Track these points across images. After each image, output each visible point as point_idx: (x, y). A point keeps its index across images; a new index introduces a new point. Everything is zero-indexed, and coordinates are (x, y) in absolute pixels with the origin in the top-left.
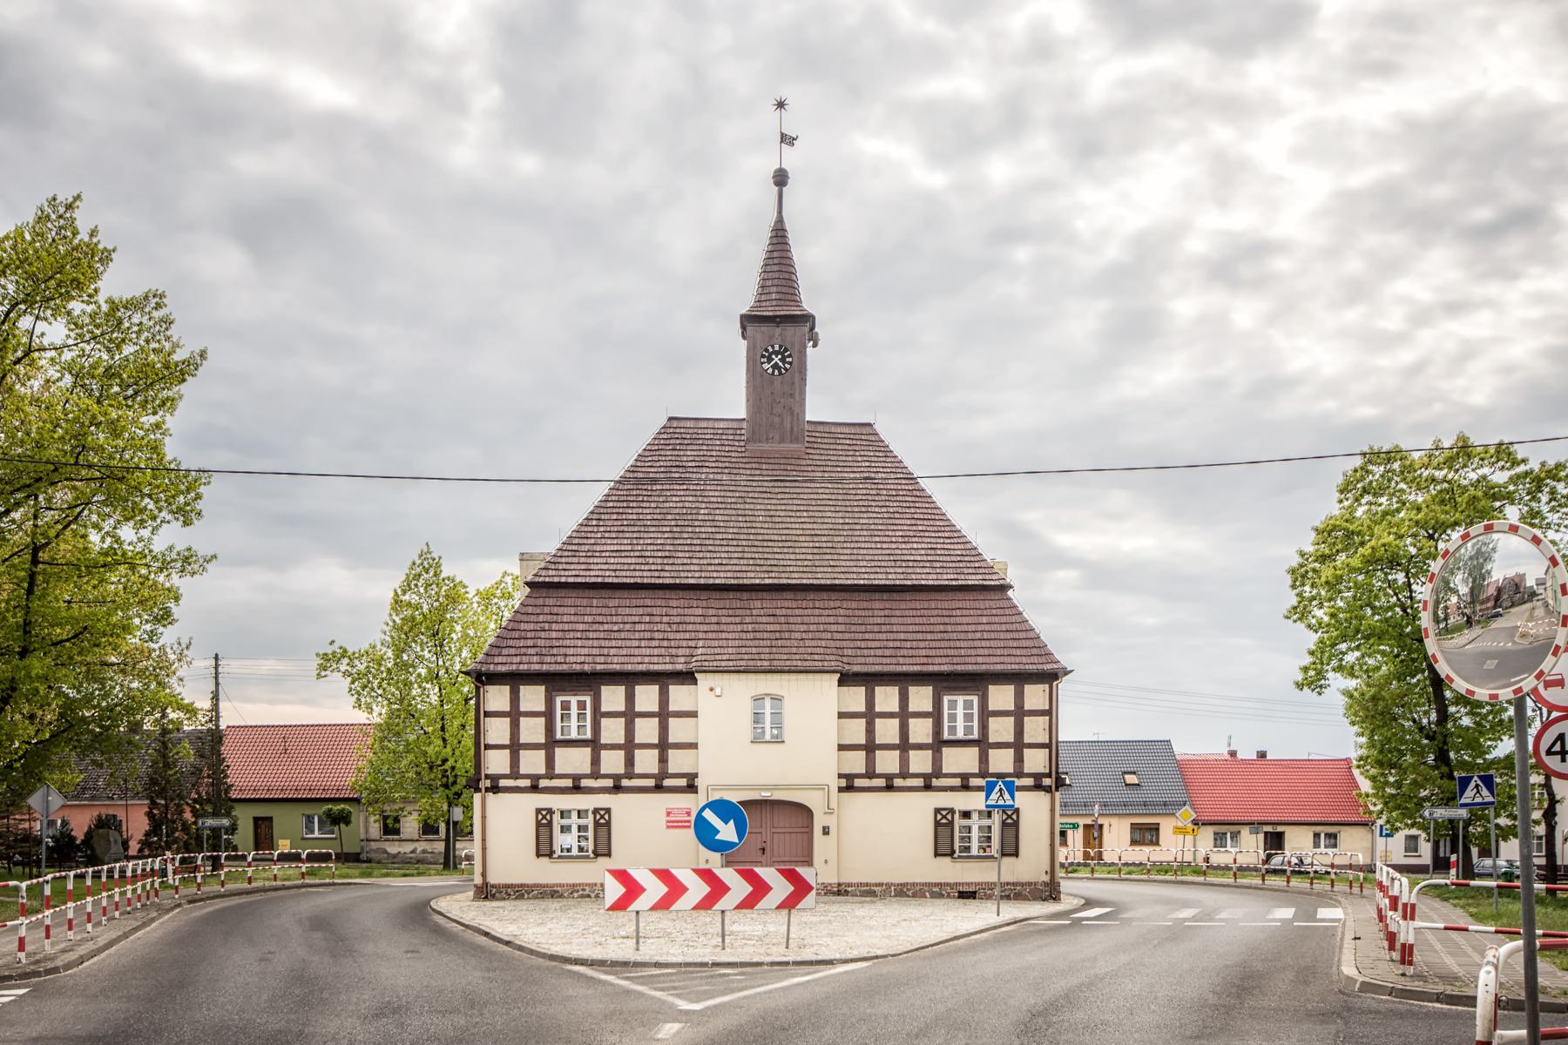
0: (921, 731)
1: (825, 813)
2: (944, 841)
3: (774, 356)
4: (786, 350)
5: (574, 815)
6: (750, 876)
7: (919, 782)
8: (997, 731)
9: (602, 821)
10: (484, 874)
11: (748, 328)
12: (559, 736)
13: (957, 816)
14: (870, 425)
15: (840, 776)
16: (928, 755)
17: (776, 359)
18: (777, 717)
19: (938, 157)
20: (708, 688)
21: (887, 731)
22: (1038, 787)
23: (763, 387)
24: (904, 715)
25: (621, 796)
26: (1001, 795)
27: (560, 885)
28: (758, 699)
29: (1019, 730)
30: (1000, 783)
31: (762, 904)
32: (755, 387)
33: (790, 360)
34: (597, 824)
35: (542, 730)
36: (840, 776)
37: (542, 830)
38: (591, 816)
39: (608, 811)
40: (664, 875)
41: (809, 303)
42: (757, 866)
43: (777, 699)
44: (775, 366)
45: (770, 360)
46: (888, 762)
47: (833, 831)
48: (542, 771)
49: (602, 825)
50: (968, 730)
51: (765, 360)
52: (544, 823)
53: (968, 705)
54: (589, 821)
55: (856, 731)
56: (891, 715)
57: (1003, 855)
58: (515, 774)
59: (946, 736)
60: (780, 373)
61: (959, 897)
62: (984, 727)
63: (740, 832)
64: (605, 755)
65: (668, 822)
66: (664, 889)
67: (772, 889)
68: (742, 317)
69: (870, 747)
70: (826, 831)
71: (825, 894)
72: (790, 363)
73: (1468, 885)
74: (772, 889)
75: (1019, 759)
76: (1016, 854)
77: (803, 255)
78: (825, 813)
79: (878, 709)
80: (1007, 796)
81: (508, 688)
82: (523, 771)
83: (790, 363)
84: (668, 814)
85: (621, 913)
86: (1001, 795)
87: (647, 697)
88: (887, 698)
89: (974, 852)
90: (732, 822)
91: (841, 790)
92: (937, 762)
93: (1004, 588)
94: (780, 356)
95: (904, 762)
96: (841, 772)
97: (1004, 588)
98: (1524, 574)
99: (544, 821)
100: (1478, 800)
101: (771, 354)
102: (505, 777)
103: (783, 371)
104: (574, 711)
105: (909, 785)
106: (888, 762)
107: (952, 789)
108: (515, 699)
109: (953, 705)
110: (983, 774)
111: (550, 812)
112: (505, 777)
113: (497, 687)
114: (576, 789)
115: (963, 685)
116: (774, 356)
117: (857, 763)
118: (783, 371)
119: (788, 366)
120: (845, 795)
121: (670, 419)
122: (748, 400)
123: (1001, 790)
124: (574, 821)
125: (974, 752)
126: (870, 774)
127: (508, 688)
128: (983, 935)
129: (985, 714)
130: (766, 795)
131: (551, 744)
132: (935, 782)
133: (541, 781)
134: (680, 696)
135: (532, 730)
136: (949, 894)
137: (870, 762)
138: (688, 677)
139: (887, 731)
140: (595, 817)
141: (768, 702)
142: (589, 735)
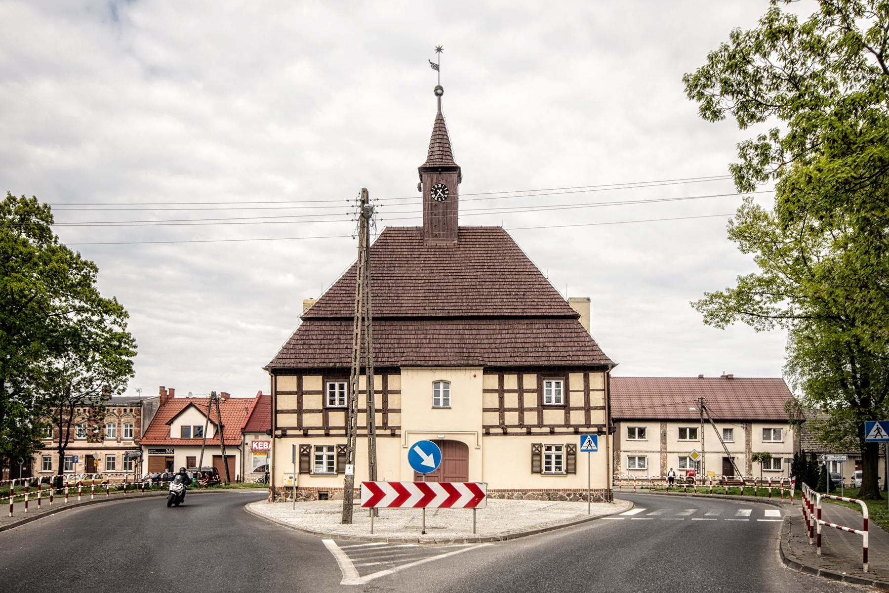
1: (476, 448)
3: (438, 190)
4: (445, 187)
6: (448, 487)
11: (423, 176)
12: (545, 403)
17: (440, 192)
18: (446, 393)
24: (587, 391)
28: (437, 383)
29: (521, 400)
30: (589, 437)
31: (405, 505)
33: (447, 192)
34: (568, 454)
36: (484, 427)
37: (303, 458)
38: (335, 449)
40: (397, 486)
41: (458, 160)
42: (455, 481)
43: (447, 383)
45: (436, 193)
50: (558, 400)
51: (433, 193)
52: (304, 454)
53: (342, 387)
54: (563, 452)
55: (493, 400)
57: (301, 473)
58: (541, 425)
60: (442, 200)
61: (320, 498)
63: (436, 461)
66: (422, 495)
67: (461, 495)
68: (419, 169)
69: (502, 410)
72: (447, 194)
74: (461, 495)
76: (575, 473)
78: (476, 448)
80: (593, 444)
81: (497, 376)
82: (572, 423)
83: (447, 194)
85: (448, 509)
88: (511, 381)
90: (431, 455)
93: (576, 317)
97: (576, 317)
101: (436, 189)
102: (534, 426)
103: (444, 199)
104: (337, 390)
106: (511, 418)
108: (520, 382)
112: (534, 426)
114: (552, 433)
116: (438, 190)
118: (444, 199)
120: (485, 438)
123: (589, 441)
127: (497, 376)
131: (541, 407)
134: (393, 382)
135: (531, 400)
137: (588, 417)
138: (396, 370)
140: (337, 450)
141: (442, 385)
142: (562, 403)
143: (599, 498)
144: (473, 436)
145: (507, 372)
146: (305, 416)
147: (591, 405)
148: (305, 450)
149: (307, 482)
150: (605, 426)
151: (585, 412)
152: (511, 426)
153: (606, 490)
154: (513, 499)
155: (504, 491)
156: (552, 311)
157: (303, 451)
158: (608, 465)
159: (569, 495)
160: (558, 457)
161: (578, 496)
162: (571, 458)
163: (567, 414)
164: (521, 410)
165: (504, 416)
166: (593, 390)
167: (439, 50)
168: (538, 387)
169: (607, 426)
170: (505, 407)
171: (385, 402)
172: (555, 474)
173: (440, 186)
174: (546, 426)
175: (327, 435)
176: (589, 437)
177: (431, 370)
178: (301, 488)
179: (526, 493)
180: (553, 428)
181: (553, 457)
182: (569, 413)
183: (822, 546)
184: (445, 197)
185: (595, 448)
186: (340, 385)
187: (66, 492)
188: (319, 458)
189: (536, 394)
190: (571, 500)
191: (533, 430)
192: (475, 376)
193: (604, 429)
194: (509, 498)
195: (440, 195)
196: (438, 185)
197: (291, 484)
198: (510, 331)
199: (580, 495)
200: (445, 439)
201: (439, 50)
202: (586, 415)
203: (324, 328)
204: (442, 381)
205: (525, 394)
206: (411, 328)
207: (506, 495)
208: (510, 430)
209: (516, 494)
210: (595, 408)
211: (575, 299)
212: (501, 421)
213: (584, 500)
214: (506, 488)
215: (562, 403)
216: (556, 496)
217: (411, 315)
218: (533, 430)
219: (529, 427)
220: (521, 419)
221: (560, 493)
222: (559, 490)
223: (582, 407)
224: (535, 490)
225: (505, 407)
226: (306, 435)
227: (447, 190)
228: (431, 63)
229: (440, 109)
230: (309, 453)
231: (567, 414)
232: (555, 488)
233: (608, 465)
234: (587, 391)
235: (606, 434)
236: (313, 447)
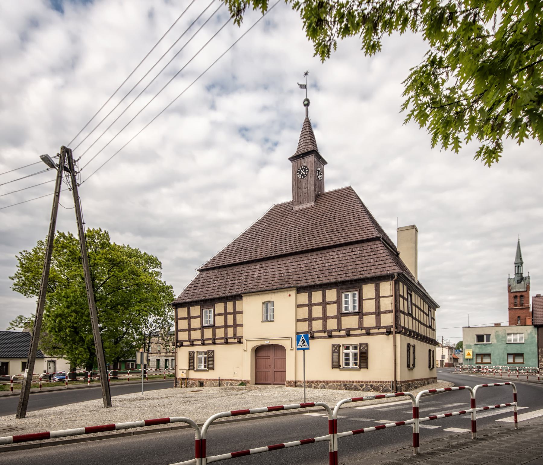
1: (291, 350)
4: (306, 167)
5: (203, 354)
12: (344, 311)
16: (217, 331)
19: (423, 71)
20: (288, 295)
22: (389, 333)
24: (378, 298)
25: (370, 337)
26: (303, 343)
28: (265, 304)
29: (324, 311)
30: (302, 336)
39: (213, 351)
44: (303, 175)
45: (300, 172)
50: (354, 307)
53: (354, 296)
55: (304, 313)
56: (333, 303)
58: (339, 329)
60: (304, 177)
64: (217, 331)
76: (367, 367)
78: (291, 350)
80: (306, 343)
83: (308, 172)
86: (303, 343)
87: (230, 305)
88: (317, 297)
89: (351, 365)
100: (303, 347)
102: (335, 330)
106: (317, 325)
108: (324, 296)
109: (346, 297)
110: (324, 331)
112: (335, 330)
114: (348, 335)
117: (304, 327)
119: (307, 173)
123: (303, 340)
124: (351, 351)
126: (378, 327)
130: (272, 342)
131: (340, 315)
133: (371, 330)
135: (332, 310)
137: (378, 320)
140: (360, 348)
142: (357, 310)
143: (388, 389)
144: (288, 340)
145: (314, 290)
146: (192, 332)
147: (381, 310)
148: (336, 349)
149: (194, 375)
150: (392, 326)
151: (376, 316)
152: (317, 331)
153: (393, 382)
154: (318, 388)
155: (312, 382)
156: (361, 237)
157: (335, 350)
158: (395, 360)
159: (362, 386)
160: (356, 354)
161: (369, 386)
162: (364, 355)
163: (361, 318)
165: (312, 324)
166: (383, 297)
167: (306, 74)
168: (337, 299)
169: (394, 327)
170: (313, 317)
171: (235, 320)
173: (303, 167)
174: (344, 330)
175: (203, 344)
176: (302, 336)
177: (259, 294)
178: (190, 379)
179: (328, 384)
181: (351, 354)
182: (362, 318)
184: (306, 175)
185: (307, 347)
187: (66, 382)
188: (200, 359)
189: (336, 305)
190: (363, 390)
191: (334, 334)
192: (290, 295)
194: (315, 387)
196: (301, 167)
197: (184, 376)
198: (323, 259)
199: (371, 386)
200: (270, 344)
201: (306, 74)
202: (376, 318)
203: (208, 275)
204: (270, 301)
205: (327, 306)
206: (257, 267)
207: (313, 385)
208: (316, 335)
209: (320, 385)
210: (385, 312)
211: (402, 228)
212: (310, 328)
213: (374, 390)
214: (313, 380)
215: (357, 310)
216: (351, 386)
218: (334, 334)
220: (325, 325)
221: (355, 384)
222: (354, 382)
223: (374, 312)
224: (335, 382)
225: (313, 317)
226: (192, 345)
227: (308, 169)
228: (299, 85)
229: (307, 115)
230: (339, 350)
231: (361, 318)
232: (351, 380)
233: (395, 360)
234: (378, 298)
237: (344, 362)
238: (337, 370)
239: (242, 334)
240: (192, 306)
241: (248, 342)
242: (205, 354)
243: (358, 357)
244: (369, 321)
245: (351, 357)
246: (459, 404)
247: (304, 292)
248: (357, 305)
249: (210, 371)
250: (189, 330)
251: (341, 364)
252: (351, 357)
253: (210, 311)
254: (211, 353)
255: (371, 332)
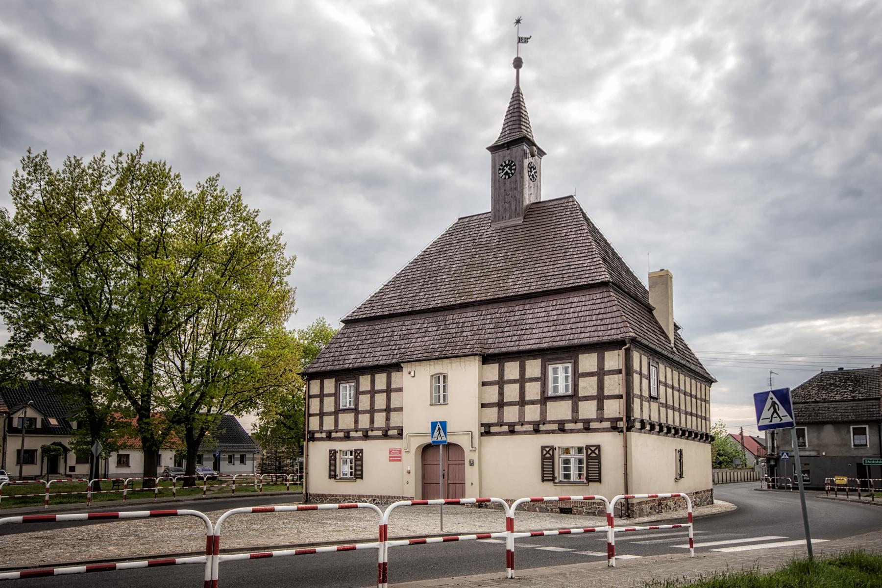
0: (533, 391)
1: (471, 451)
2: (548, 470)
4: (512, 162)
5: (349, 453)
7: (530, 428)
8: (585, 388)
9: (593, 455)
10: (307, 489)
13: (556, 452)
14: (572, 196)
15: (482, 425)
16: (537, 407)
21: (380, 401)
22: (614, 428)
23: (500, 188)
27: (339, 495)
29: (601, 386)
32: (496, 189)
35: (333, 404)
39: (362, 451)
44: (507, 173)
45: (503, 170)
46: (511, 414)
47: (476, 463)
48: (333, 428)
49: (359, 459)
50: (567, 390)
55: (492, 394)
56: (514, 382)
59: (551, 393)
60: (509, 177)
62: (575, 386)
65: (390, 457)
70: (472, 464)
71: (471, 506)
73: (681, 526)
75: (600, 408)
77: (530, 106)
78: (471, 451)
79: (506, 378)
83: (515, 170)
84: (390, 452)
86: (775, 411)
87: (381, 380)
88: (512, 370)
89: (574, 477)
91: (482, 435)
92: (543, 413)
94: (509, 167)
95: (522, 414)
96: (484, 422)
98: (488, 149)
99: (548, 455)
102: (352, 430)
103: (511, 175)
105: (525, 430)
107: (553, 432)
108: (601, 361)
109: (555, 371)
111: (553, 448)
112: (352, 430)
113: (315, 381)
115: (562, 356)
117: (491, 415)
118: (511, 175)
119: (513, 171)
120: (484, 438)
121: (460, 219)
122: (492, 198)
123: (774, 404)
125: (568, 404)
127: (595, 355)
128: (579, 535)
129: (577, 376)
132: (542, 427)
135: (614, 385)
136: (552, 509)
137: (501, 415)
139: (512, 392)
140: (355, 454)
148: (548, 452)
150: (621, 419)
157: (546, 454)
164: (600, 398)
172: (574, 482)
174: (505, 424)
180: (348, 433)
181: (572, 461)
183: (206, 536)
186: (553, 369)
193: (621, 424)
195: (507, 171)
196: (505, 162)
215: (570, 392)
217: (400, 311)
219: (587, 422)
227: (515, 165)
235: (622, 431)
236: (557, 449)
237: (562, 473)
238: (550, 484)
239: (402, 423)
240: (327, 378)
241: (412, 439)
242: (351, 455)
243: (584, 465)
244: (588, 410)
245: (573, 465)
246: (639, 543)
247: (316, 379)
248: (570, 383)
249: (358, 480)
250: (522, 402)
251: (556, 475)
252: (573, 465)
253: (350, 386)
254: (359, 454)
255: (566, 428)
